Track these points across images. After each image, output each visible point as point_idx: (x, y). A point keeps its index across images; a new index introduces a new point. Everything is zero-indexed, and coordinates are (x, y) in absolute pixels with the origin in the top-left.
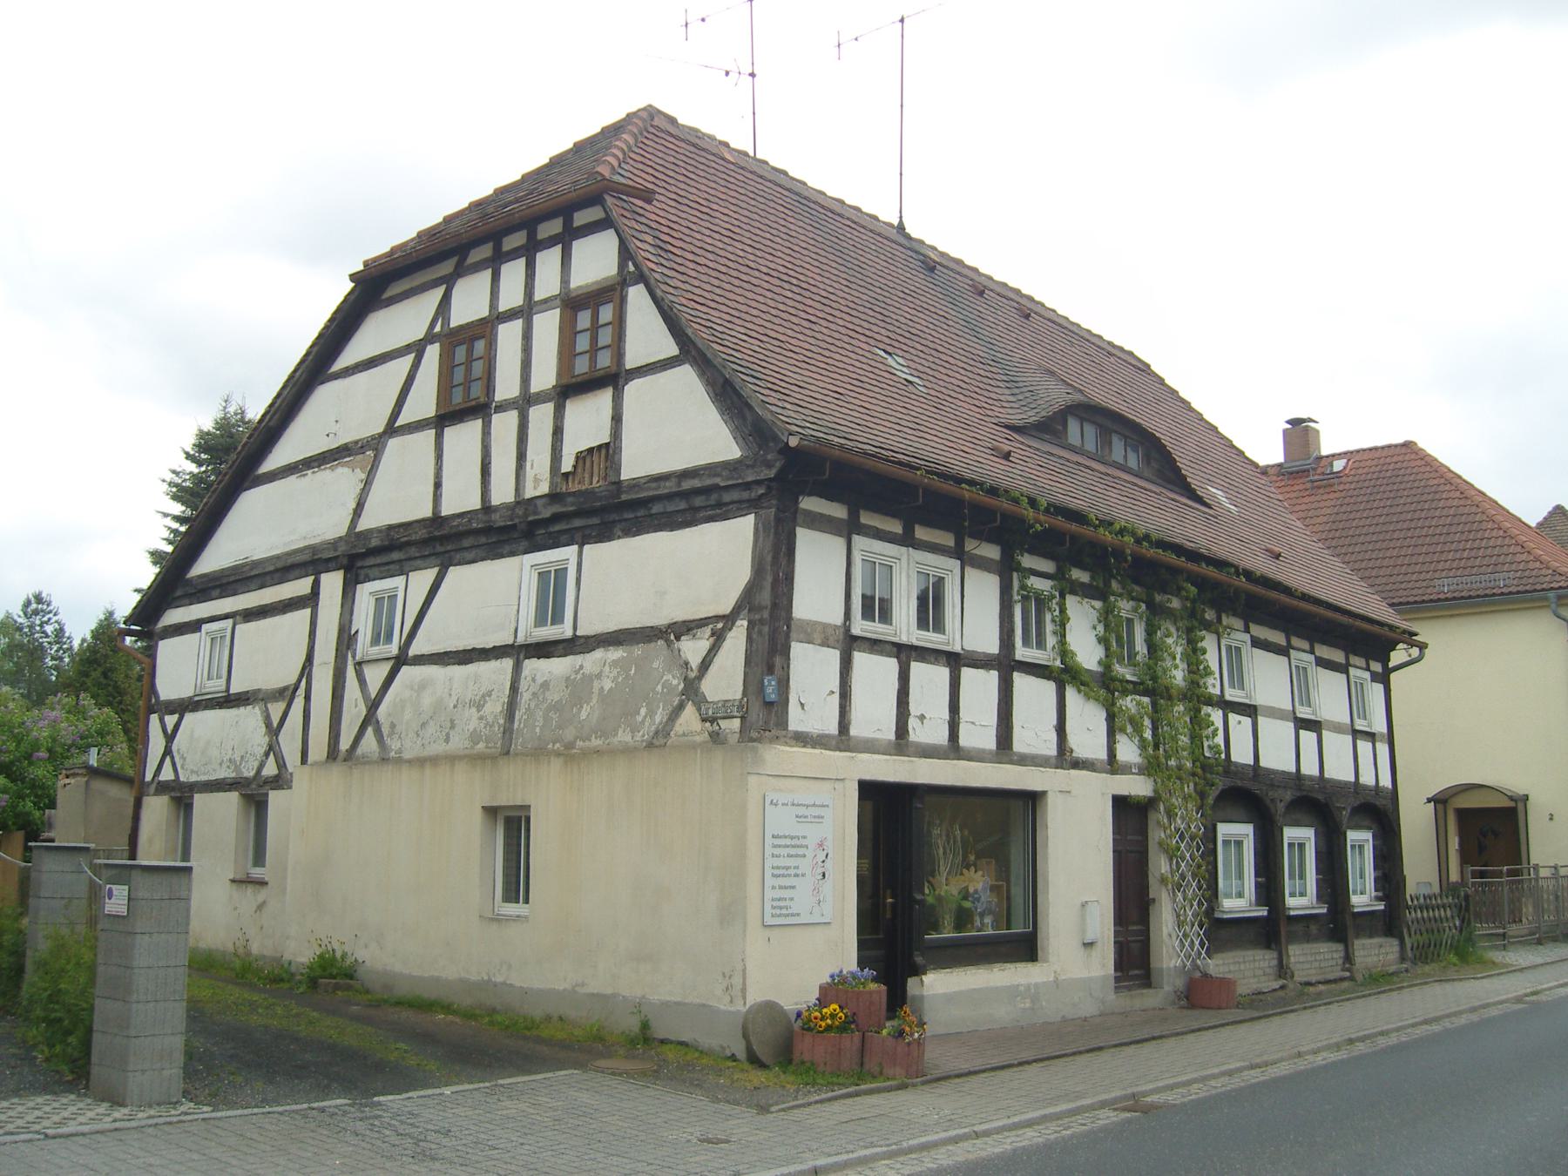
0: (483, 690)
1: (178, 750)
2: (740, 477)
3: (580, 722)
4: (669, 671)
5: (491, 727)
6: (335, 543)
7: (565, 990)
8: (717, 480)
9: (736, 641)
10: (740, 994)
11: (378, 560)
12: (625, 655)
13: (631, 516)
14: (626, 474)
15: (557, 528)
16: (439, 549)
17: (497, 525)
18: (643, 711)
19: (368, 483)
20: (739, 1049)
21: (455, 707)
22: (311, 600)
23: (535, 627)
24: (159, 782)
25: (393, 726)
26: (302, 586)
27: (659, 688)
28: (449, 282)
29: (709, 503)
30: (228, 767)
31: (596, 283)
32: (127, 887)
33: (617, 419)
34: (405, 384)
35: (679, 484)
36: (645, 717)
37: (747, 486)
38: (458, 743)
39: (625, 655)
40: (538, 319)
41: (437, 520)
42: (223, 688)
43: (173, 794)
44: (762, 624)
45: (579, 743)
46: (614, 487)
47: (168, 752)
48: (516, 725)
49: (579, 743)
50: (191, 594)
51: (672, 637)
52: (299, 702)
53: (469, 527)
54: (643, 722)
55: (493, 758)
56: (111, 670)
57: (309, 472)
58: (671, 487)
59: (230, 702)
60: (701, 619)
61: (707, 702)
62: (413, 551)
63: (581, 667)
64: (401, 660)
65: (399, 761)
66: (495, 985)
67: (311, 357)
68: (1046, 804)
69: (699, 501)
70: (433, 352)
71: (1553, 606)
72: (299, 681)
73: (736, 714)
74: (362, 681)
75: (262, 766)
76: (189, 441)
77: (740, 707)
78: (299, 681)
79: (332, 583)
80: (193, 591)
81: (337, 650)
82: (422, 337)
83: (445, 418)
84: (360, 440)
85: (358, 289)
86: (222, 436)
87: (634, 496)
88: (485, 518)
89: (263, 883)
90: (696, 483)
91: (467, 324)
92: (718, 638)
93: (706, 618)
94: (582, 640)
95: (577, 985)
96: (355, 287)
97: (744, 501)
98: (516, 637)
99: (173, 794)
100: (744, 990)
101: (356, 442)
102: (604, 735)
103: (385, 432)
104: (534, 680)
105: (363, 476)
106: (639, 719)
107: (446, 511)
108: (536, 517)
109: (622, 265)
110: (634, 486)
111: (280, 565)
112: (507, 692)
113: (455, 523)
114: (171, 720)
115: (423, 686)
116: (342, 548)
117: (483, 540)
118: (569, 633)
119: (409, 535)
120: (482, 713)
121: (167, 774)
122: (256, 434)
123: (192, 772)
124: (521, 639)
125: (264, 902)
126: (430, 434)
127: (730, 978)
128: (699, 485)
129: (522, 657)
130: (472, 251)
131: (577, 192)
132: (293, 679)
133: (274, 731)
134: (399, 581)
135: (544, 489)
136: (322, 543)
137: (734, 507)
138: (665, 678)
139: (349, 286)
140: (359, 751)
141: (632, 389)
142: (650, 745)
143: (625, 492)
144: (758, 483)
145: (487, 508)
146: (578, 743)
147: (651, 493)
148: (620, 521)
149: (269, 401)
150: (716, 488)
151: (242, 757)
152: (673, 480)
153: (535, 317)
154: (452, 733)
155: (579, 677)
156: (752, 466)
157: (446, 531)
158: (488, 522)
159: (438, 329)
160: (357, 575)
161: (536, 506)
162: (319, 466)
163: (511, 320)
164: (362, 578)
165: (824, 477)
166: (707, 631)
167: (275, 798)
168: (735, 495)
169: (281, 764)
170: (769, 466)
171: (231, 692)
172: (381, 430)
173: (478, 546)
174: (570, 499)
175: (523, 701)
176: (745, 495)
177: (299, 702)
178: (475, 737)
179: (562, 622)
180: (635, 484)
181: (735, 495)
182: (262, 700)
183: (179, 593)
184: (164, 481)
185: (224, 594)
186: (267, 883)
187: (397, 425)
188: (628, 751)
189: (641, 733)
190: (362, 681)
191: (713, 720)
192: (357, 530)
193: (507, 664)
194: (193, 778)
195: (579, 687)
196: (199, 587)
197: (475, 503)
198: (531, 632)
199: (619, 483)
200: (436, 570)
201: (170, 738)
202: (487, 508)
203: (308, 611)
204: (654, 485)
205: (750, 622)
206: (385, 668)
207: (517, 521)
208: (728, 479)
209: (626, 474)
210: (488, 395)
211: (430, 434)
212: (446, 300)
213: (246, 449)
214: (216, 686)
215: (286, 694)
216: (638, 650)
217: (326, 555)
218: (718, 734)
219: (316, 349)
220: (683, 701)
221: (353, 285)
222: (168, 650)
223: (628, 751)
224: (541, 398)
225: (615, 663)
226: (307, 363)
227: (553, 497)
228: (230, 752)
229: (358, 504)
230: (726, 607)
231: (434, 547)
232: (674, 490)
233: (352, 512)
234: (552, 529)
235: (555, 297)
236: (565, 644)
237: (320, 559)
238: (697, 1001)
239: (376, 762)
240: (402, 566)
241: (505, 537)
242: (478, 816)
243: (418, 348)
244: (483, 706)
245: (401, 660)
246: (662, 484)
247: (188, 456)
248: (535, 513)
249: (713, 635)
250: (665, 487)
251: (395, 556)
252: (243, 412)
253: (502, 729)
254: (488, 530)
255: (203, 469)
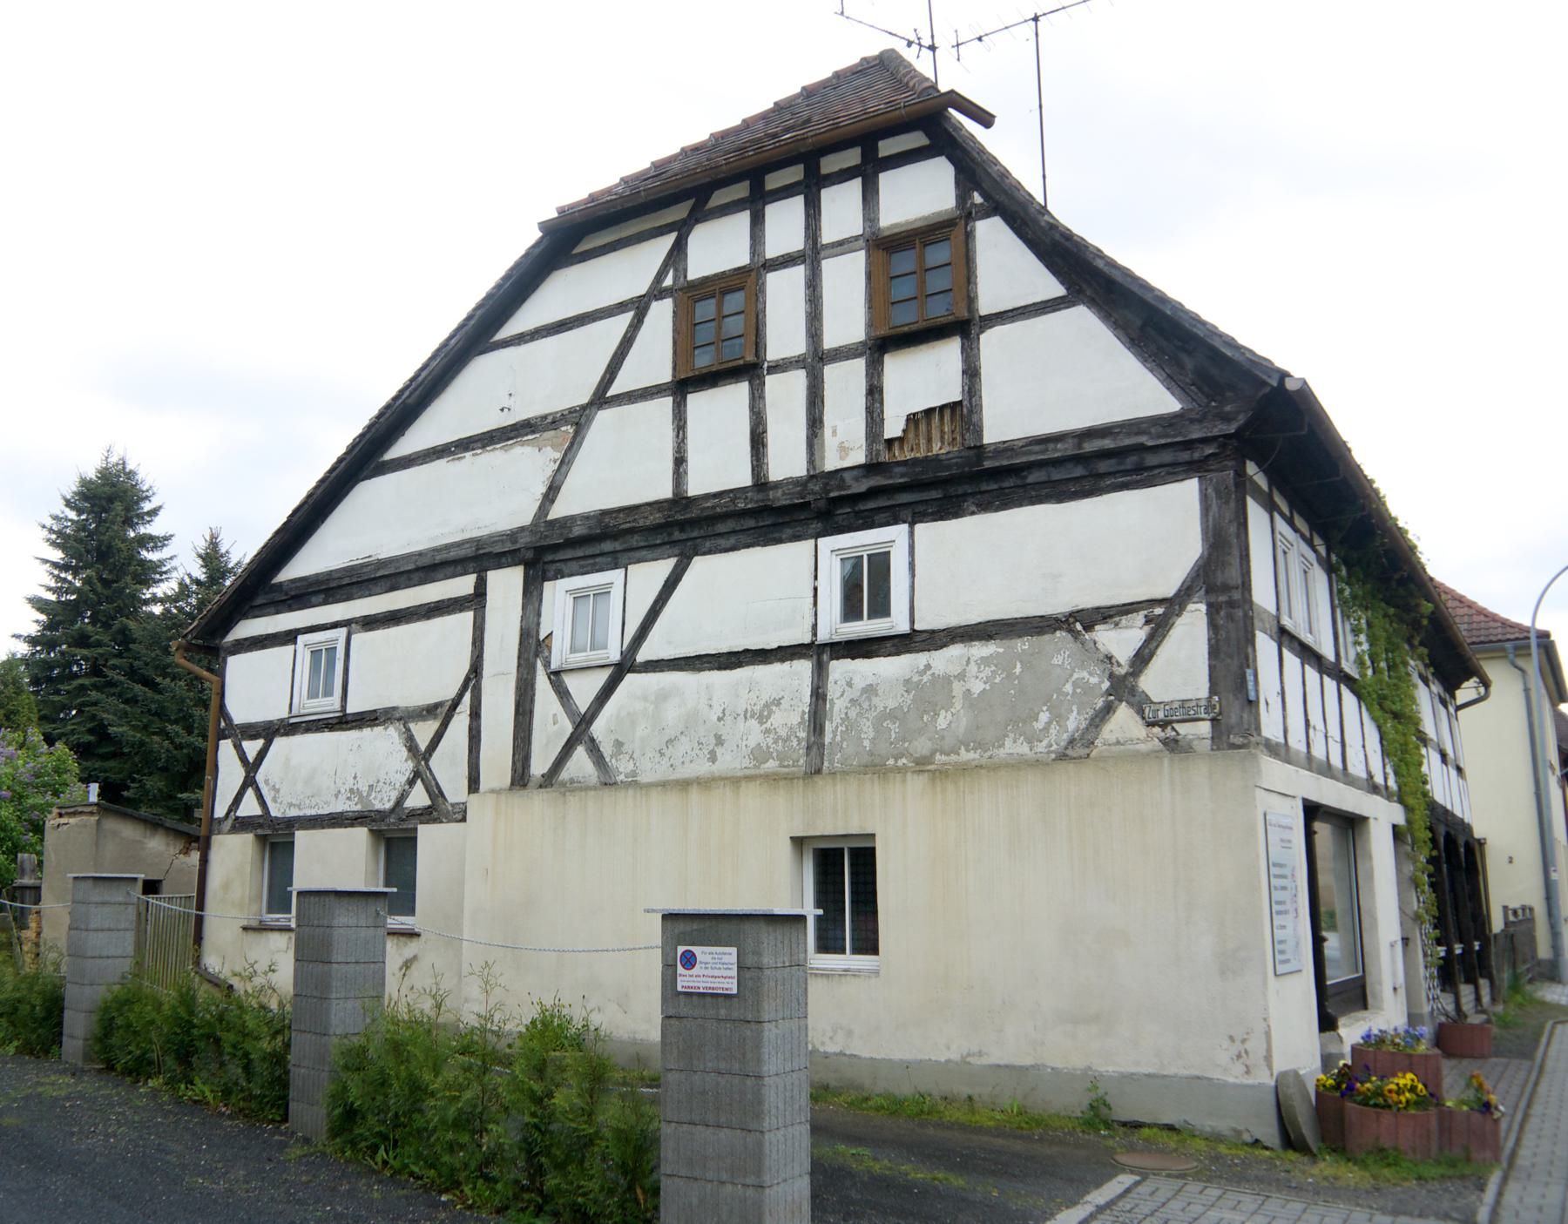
0: (765, 698)
1: (267, 782)
2: (1180, 434)
3: (937, 732)
4: (1082, 667)
5: (785, 741)
6: (513, 535)
7: (948, 1061)
8: (1143, 439)
9: (1192, 628)
10: (1262, 1062)
11: (579, 553)
12: (1001, 650)
13: (995, 487)
14: (990, 437)
15: (871, 505)
16: (677, 535)
17: (778, 504)
18: (1044, 717)
19: (565, 464)
20: (1268, 1132)
21: (719, 719)
22: (477, 600)
23: (308, 698)
24: (237, 818)
25: (619, 744)
26: (463, 585)
27: (1068, 688)
28: (683, 230)
29: (1122, 468)
30: (349, 798)
31: (907, 223)
32: (734, 950)
33: (971, 373)
34: (619, 348)
35: (1079, 446)
36: (1049, 724)
37: (1188, 445)
38: (731, 761)
39: (1001, 650)
40: (828, 266)
41: (680, 501)
42: (337, 706)
43: (260, 832)
44: (1233, 607)
45: (939, 758)
46: (972, 453)
47: (250, 782)
48: (828, 738)
49: (939, 758)
50: (282, 601)
51: (1079, 627)
52: (461, 722)
53: (732, 508)
54: (1046, 729)
55: (789, 778)
56: (15, 713)
57: (468, 455)
58: (1066, 449)
59: (347, 723)
60: (1124, 605)
61: (1152, 702)
62: (635, 540)
63: (928, 667)
64: (624, 667)
65: (633, 784)
66: (826, 1056)
67: (472, 322)
68: (1369, 833)
69: (1103, 466)
70: (661, 314)
71: (1511, 656)
72: (460, 695)
73: (1203, 716)
74: (563, 694)
75: (403, 797)
76: (70, 487)
77: (1209, 706)
78: (460, 695)
79: (506, 584)
80: (285, 598)
81: (519, 658)
82: (643, 293)
83: (683, 386)
84: (550, 414)
85: (545, 242)
86: (104, 485)
87: (1005, 463)
88: (761, 496)
89: (412, 935)
90: (1107, 443)
91: (715, 275)
92: (1159, 629)
93: (1132, 604)
94: (924, 636)
95: (969, 1055)
96: (542, 238)
97: (1180, 464)
98: (815, 634)
99: (260, 832)
100: (1268, 1058)
101: (545, 417)
102: (980, 745)
103: (591, 404)
104: (850, 684)
105: (558, 456)
106: (1039, 725)
107: (694, 488)
108: (843, 493)
109: (962, 196)
110: (1006, 450)
111: (422, 562)
112: (808, 700)
113: (709, 504)
114: (252, 747)
115: (663, 696)
116: (524, 540)
117: (751, 523)
118: (904, 628)
119: (634, 520)
120: (768, 725)
121: (249, 807)
122: (390, 412)
123: (291, 805)
124: (823, 636)
125: (415, 957)
126: (667, 402)
127: (1244, 1041)
128: (1112, 446)
129: (825, 657)
130: (717, 193)
131: (907, 109)
132: (450, 693)
133: (421, 757)
134: (615, 576)
135: (858, 457)
136: (490, 536)
137: (1163, 471)
138: (1076, 676)
139: (537, 234)
140: (565, 775)
141: (991, 342)
142: (1062, 757)
143: (989, 458)
144: (1204, 441)
145: (761, 483)
146: (938, 756)
147: (1032, 458)
148: (973, 494)
149: (411, 374)
150: (1141, 448)
151: (371, 787)
152: (1070, 441)
153: (824, 263)
154: (719, 751)
155: (925, 679)
156: (1200, 421)
157: (694, 513)
158: (763, 501)
159: (668, 281)
160: (544, 571)
161: (842, 479)
162: (483, 447)
163: (785, 267)
164: (551, 574)
165: (1303, 433)
166: (1139, 618)
167: (427, 835)
168: (1167, 457)
169: (436, 793)
170: (1227, 418)
171: (348, 711)
172: (585, 400)
173: (742, 531)
174: (898, 470)
175: (836, 709)
176: (1185, 456)
177: (461, 722)
178: (759, 754)
179: (332, 695)
180: (1006, 448)
181: (1167, 457)
182: (399, 719)
183: (260, 601)
184: (44, 527)
185: (330, 600)
186: (418, 935)
187: (609, 394)
188: (1019, 765)
189: (1045, 743)
190: (563, 694)
191: (1164, 724)
192: (550, 517)
193: (804, 668)
194: (293, 813)
195: (930, 695)
196: (293, 593)
197: (744, 479)
198: (833, 626)
199: (980, 449)
200: (672, 562)
201: (252, 768)
202: (761, 483)
203: (468, 616)
204: (1036, 448)
205: (1210, 606)
206: (602, 677)
207: (809, 498)
208: (1159, 437)
209: (990, 437)
210: (757, 354)
211: (667, 402)
212: (678, 252)
213: (373, 430)
214: (328, 705)
215: (442, 712)
216: (1022, 645)
217: (498, 549)
218: (1176, 741)
219: (479, 313)
220: (1111, 701)
221: (541, 234)
222: (238, 668)
223: (1019, 765)
224: (843, 354)
225: (985, 661)
226: (466, 328)
227: (870, 468)
228: (351, 781)
229: (550, 488)
230: (1169, 588)
231: (670, 535)
232: (1069, 453)
233: (541, 497)
234: (861, 507)
235: (856, 238)
236: (896, 641)
237: (489, 554)
238: (1186, 1073)
239: (594, 788)
240: (616, 558)
241: (787, 519)
242: (786, 848)
243: (639, 307)
244: (768, 717)
245: (624, 667)
246: (1051, 446)
247: (68, 503)
248: (841, 488)
249: (1147, 622)
250: (1056, 450)
251: (607, 546)
252: (124, 463)
253: (804, 744)
254: (764, 510)
255: (83, 517)
